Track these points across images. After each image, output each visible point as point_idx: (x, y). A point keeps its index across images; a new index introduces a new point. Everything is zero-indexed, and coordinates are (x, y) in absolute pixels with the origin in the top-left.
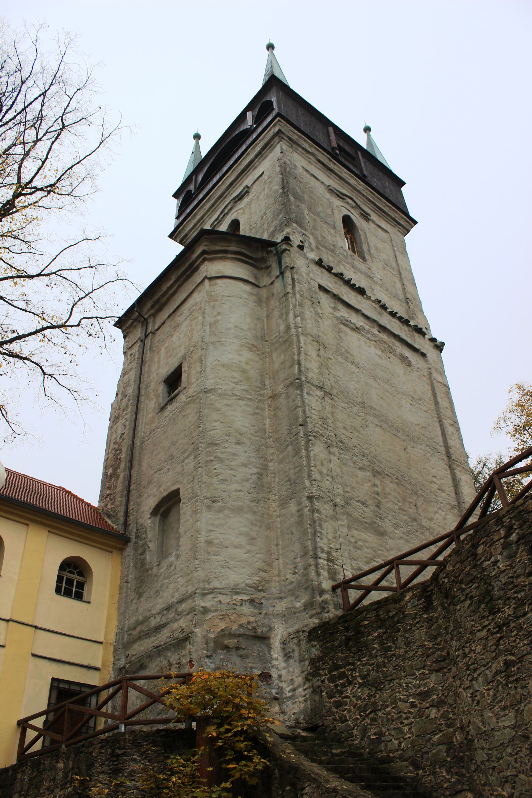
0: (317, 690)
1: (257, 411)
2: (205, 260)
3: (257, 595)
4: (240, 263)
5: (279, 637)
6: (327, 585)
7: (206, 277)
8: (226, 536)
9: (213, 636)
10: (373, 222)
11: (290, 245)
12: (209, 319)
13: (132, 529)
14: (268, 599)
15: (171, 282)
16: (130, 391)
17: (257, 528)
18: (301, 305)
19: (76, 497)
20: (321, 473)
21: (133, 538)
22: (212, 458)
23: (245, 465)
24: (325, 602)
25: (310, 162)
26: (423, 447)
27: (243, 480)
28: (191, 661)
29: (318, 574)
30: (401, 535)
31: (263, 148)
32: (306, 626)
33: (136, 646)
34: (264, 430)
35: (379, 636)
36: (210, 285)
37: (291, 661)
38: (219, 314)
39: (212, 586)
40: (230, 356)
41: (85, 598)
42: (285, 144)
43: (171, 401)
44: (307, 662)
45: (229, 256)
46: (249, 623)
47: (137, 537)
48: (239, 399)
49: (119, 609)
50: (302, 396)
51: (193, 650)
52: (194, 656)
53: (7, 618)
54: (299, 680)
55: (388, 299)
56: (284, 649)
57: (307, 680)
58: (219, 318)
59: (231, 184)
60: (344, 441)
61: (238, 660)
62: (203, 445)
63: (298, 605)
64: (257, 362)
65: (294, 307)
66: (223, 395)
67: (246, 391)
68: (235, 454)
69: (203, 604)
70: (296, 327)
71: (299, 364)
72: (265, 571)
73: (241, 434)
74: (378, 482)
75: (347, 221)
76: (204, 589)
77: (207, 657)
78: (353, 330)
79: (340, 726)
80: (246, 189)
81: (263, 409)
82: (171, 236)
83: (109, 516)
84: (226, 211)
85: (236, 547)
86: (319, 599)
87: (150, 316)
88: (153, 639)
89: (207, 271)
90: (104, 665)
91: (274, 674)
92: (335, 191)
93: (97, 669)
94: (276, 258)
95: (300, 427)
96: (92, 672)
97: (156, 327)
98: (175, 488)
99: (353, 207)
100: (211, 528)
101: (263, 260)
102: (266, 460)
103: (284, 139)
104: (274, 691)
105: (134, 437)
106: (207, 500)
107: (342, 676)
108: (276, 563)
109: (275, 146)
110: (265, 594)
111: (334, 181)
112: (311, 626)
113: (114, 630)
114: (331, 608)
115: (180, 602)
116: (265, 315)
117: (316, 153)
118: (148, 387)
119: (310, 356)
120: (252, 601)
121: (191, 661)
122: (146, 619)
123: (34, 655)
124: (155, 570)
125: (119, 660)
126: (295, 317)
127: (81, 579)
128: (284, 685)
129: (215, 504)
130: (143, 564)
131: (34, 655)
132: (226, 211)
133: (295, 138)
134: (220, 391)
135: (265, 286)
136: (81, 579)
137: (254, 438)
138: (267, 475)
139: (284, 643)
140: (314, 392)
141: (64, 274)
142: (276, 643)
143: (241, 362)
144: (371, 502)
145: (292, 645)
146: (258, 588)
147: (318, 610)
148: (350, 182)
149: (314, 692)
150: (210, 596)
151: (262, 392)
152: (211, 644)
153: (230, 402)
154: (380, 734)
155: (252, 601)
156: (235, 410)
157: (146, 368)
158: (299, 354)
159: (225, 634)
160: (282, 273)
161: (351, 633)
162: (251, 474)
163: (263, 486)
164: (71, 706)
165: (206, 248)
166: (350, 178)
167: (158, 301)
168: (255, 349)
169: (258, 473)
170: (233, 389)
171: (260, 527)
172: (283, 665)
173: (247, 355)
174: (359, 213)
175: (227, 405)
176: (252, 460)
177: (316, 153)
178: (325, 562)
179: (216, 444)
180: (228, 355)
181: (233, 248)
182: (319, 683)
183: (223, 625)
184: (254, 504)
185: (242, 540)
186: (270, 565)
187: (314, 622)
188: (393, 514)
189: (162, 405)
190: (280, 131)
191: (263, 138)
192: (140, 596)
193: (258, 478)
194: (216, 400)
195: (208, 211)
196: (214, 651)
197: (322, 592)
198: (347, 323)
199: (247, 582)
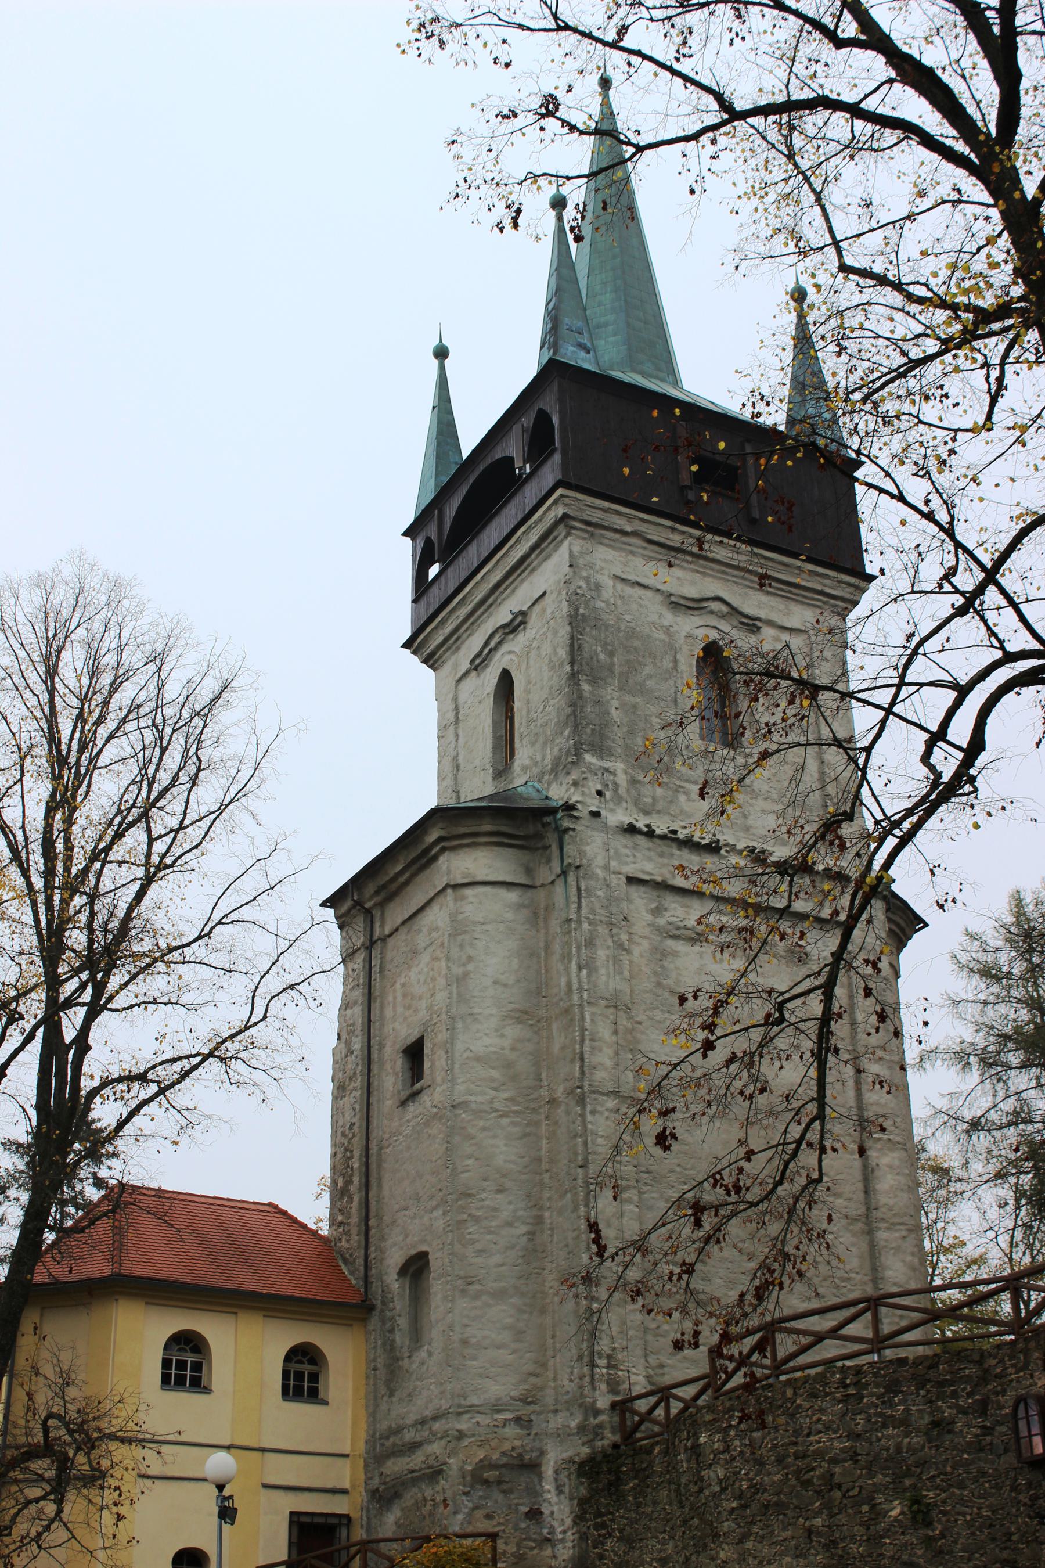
0: (583, 1537)
1: (528, 1130)
2: (444, 850)
3: (525, 1410)
4: (501, 849)
5: (552, 1463)
6: (603, 1402)
7: (447, 886)
8: (486, 1333)
9: (470, 1468)
11: (577, 818)
12: (458, 970)
13: (376, 1287)
14: (539, 1413)
15: (399, 867)
16: (357, 1045)
17: (525, 1316)
18: (590, 943)
19: (294, 1220)
21: (378, 1303)
22: (465, 1217)
23: (509, 1224)
24: (600, 1426)
25: (632, 552)
27: (507, 1248)
28: (445, 1500)
29: (594, 1388)
32: (578, 1454)
33: (389, 1463)
34: (539, 1160)
35: (633, 1488)
36: (456, 900)
37: (562, 1497)
38: (470, 959)
39: (468, 1403)
40: (487, 1041)
41: (321, 1395)
42: (578, 537)
43: (414, 1095)
46: (513, 1448)
47: (383, 1303)
48: (501, 1116)
49: (367, 1407)
50: (583, 1116)
51: (447, 1487)
52: (449, 1494)
53: (228, 1443)
54: (569, 1522)
56: (556, 1480)
57: (575, 1523)
58: (470, 967)
61: (500, 1497)
62: (453, 1197)
63: (573, 1424)
64: (529, 1040)
65: (579, 948)
66: (478, 1113)
67: (511, 1100)
68: (495, 1209)
69: (459, 1427)
70: (580, 989)
71: (582, 1059)
72: (536, 1375)
73: (504, 1176)
76: (459, 1406)
77: (465, 1494)
78: (692, 941)
80: (520, 618)
81: (537, 1124)
82: (407, 645)
83: (345, 1261)
84: (493, 644)
85: (499, 1347)
86: (593, 1421)
87: (375, 905)
88: (408, 1459)
89: (449, 872)
90: (353, 1486)
91: (546, 1511)
92: (682, 602)
93: (344, 1492)
94: (556, 835)
95: (580, 1170)
96: (339, 1497)
97: (387, 932)
99: (723, 617)
100: (466, 1321)
101: (539, 836)
102: (541, 1208)
103: (575, 528)
104: (545, 1531)
105: (368, 1139)
106: (460, 1282)
107: (603, 1525)
108: (551, 1363)
109: (562, 542)
110: (536, 1408)
111: (685, 569)
112: (583, 1456)
113: (363, 1436)
114: (608, 1433)
115: (435, 1418)
116: (542, 944)
117: (642, 528)
118: (381, 1046)
119: (600, 1039)
120: (518, 1420)
121: (445, 1500)
122: (398, 1430)
123: (265, 1486)
124: (405, 1363)
125: (371, 1478)
126: (580, 968)
128: (555, 1524)
129: (471, 1287)
130: (392, 1349)
131: (265, 1486)
132: (493, 644)
133: (596, 516)
134: (473, 1106)
135: (543, 885)
136: (312, 1368)
137: (523, 1177)
138: (542, 1231)
139: (556, 1472)
140: (602, 1105)
141: (234, 916)
143: (503, 1049)
145: (563, 1477)
146: (525, 1400)
147: (591, 1437)
148: (718, 557)
149: (581, 1538)
150: (466, 1416)
151: (535, 1095)
152: (468, 1478)
153: (488, 1124)
155: (518, 1420)
156: (495, 1137)
157: (376, 1006)
158: (583, 1041)
159: (485, 1465)
160: (564, 873)
162: (518, 1237)
163: (535, 1251)
164: (313, 1562)
165: (442, 833)
167: (383, 887)
168: (526, 1017)
169: (529, 1233)
170: (491, 1101)
171: (531, 1313)
172: (555, 1499)
173: (512, 1032)
174: (736, 623)
175: (484, 1129)
176: (521, 1213)
177: (642, 528)
178: (604, 1371)
179: (469, 1195)
180: (485, 1038)
181: (487, 828)
182: (584, 1529)
183: (481, 1454)
184: (522, 1281)
185: (506, 1336)
186: (544, 1365)
187: (586, 1450)
188: (730, 1266)
189: (403, 1098)
190: (565, 516)
191: (540, 519)
192: (391, 1394)
193: (529, 1240)
194: (469, 1121)
196: (472, 1487)
197: (597, 1412)
198: (678, 932)
199: (512, 1394)
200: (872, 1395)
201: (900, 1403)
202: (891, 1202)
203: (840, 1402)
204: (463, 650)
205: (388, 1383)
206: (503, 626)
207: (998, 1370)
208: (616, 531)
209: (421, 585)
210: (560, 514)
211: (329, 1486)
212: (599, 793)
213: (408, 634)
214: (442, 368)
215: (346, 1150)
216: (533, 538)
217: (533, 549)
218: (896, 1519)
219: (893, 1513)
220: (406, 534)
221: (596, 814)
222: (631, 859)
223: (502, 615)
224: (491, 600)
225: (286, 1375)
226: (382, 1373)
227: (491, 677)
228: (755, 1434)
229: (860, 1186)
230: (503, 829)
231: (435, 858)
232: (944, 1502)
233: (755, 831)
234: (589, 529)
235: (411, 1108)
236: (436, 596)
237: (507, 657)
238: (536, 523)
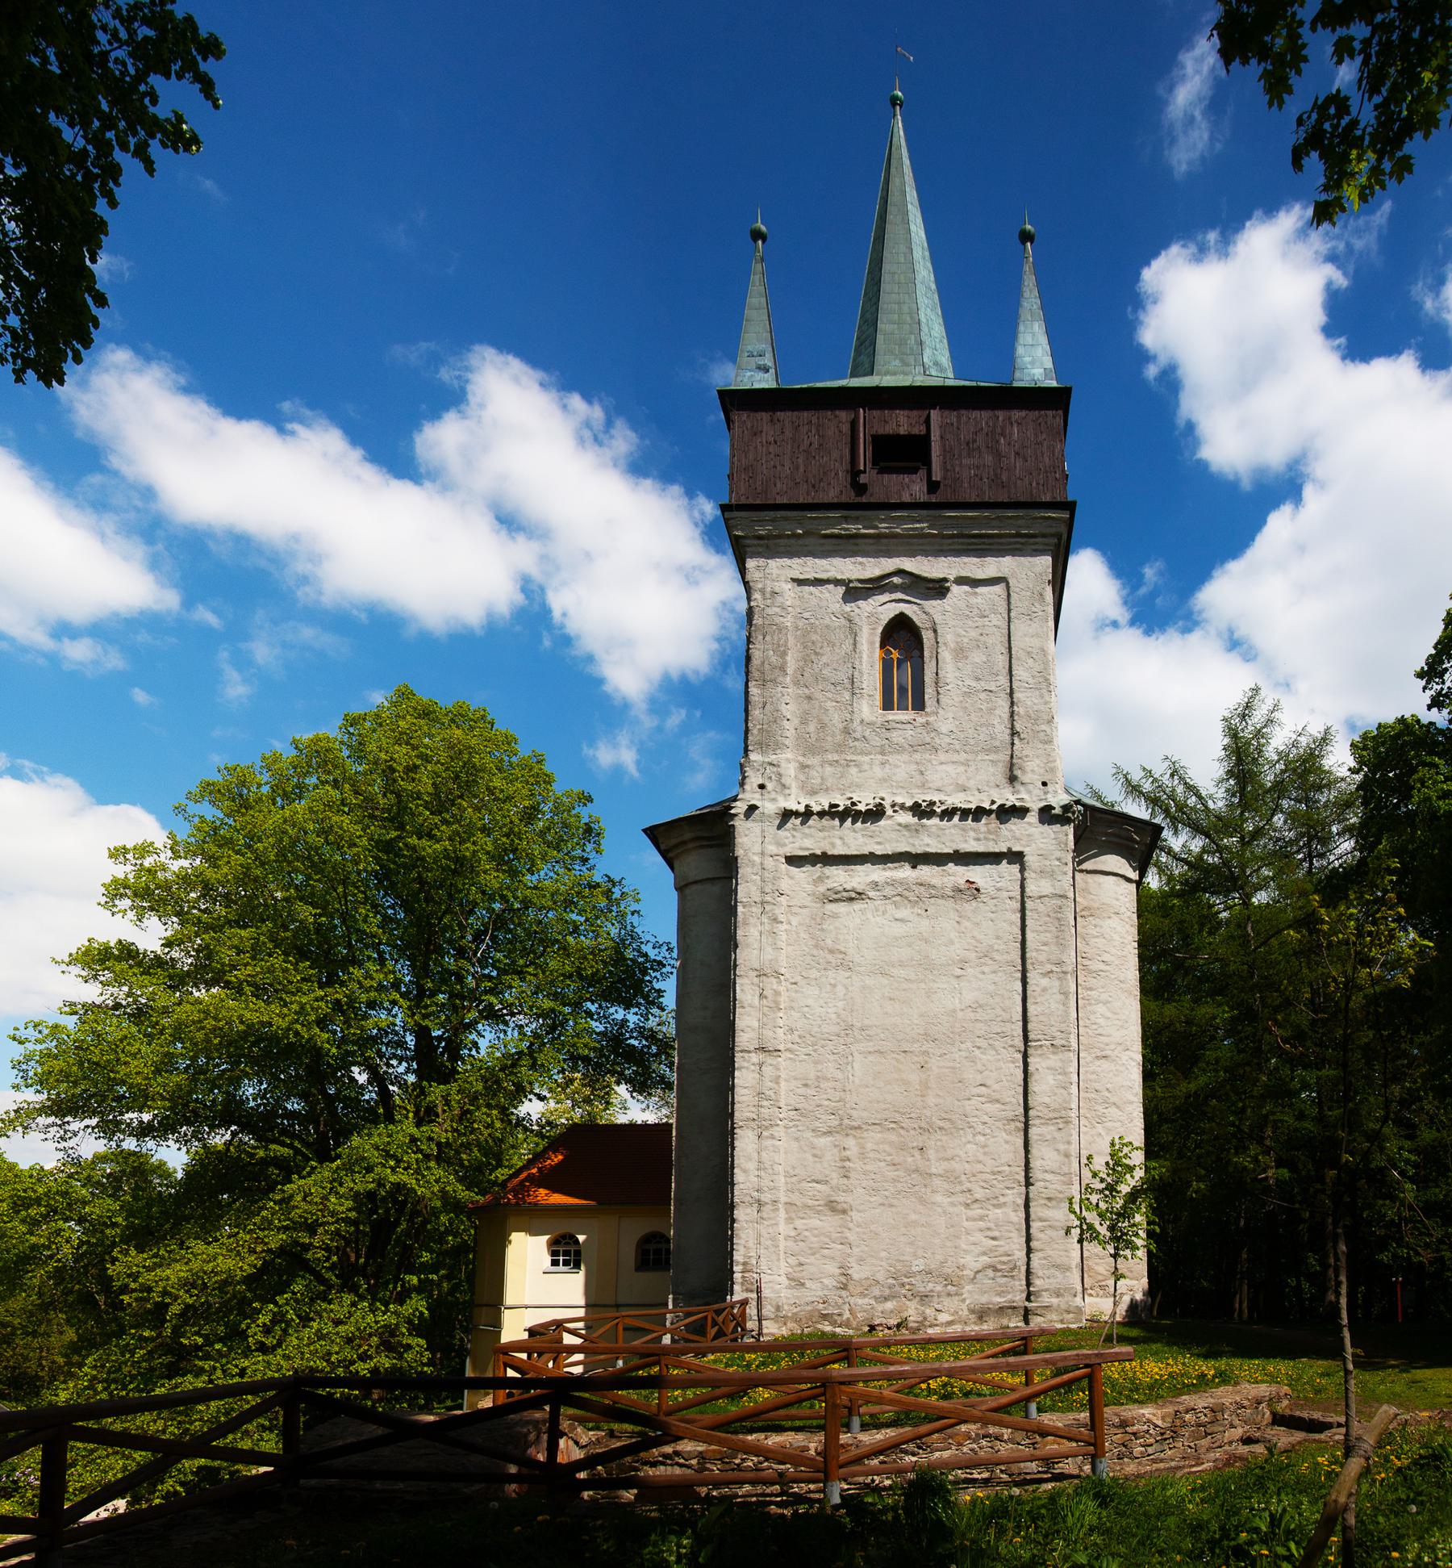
20: (745, 1171)
30: (881, 1201)
45: (691, 845)
55: (962, 769)
60: (798, 1106)
181: (688, 836)
202: (1047, 1100)
222: (791, 839)
233: (931, 785)
234: (762, 542)
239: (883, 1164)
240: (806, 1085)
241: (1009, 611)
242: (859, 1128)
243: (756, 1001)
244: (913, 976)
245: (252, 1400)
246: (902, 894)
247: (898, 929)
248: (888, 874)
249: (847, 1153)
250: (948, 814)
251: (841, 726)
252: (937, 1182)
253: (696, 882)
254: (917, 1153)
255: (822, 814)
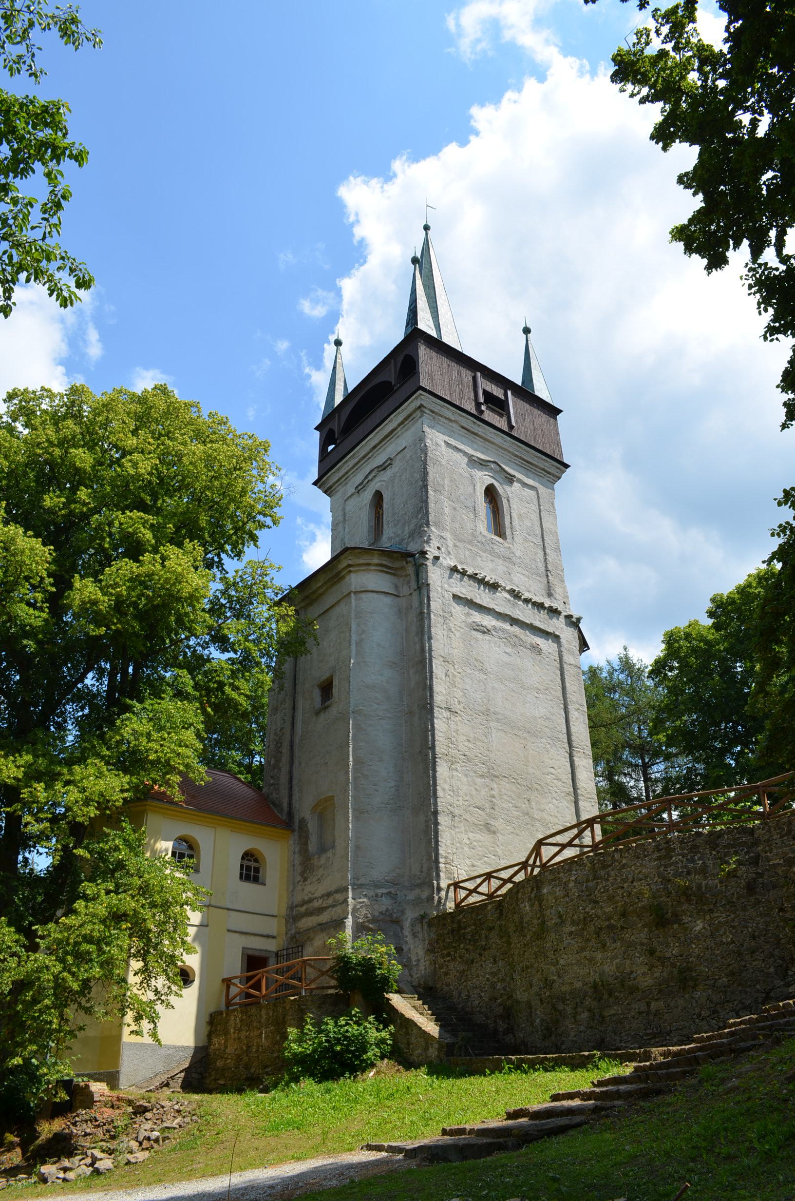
2: (350, 572)
5: (409, 920)
10: (520, 481)
20: (444, 790)
26: (543, 740)
30: (512, 830)
31: (406, 419)
33: (304, 920)
41: (260, 880)
44: (427, 942)
45: (373, 568)
55: (526, 579)
58: (363, 636)
59: (375, 447)
60: (466, 753)
74: (495, 786)
75: (491, 493)
79: (446, 988)
80: (389, 462)
82: (315, 484)
84: (370, 477)
93: (274, 937)
98: (330, 794)
107: (449, 954)
122: (311, 901)
123: (229, 931)
127: (256, 865)
131: (229, 931)
136: (256, 865)
142: (407, 924)
144: (487, 805)
145: (418, 928)
148: (495, 441)
154: (469, 996)
155: (389, 893)
161: (455, 926)
166: (495, 437)
172: (412, 941)
190: (421, 406)
192: (305, 880)
195: (352, 468)
200: (679, 855)
201: (699, 859)
203: (655, 860)
204: (349, 484)
205: (302, 874)
206: (378, 467)
207: (767, 837)
208: (446, 418)
209: (324, 454)
210: (418, 405)
211: (265, 933)
212: (439, 548)
213: (316, 477)
214: (427, 234)
215: (277, 743)
216: (400, 418)
217: (399, 425)
218: (700, 932)
219: (698, 928)
220: (316, 428)
221: (437, 558)
223: (380, 459)
224: (369, 455)
225: (242, 866)
226: (299, 869)
227: (368, 495)
228: (590, 884)
229: (570, 776)
230: (385, 563)
231: (343, 577)
232: (733, 920)
235: (322, 716)
236: (330, 461)
237: (379, 484)
238: (403, 410)
239: (511, 805)
240: (468, 741)
241: (539, 505)
242: (497, 777)
243: (444, 677)
244: (515, 689)
245: (517, 868)
246: (508, 639)
247: (506, 659)
248: (501, 625)
249: (493, 792)
250: (527, 601)
251: (471, 531)
252: (538, 824)
253: (373, 592)
254: (527, 802)
255: (470, 577)
